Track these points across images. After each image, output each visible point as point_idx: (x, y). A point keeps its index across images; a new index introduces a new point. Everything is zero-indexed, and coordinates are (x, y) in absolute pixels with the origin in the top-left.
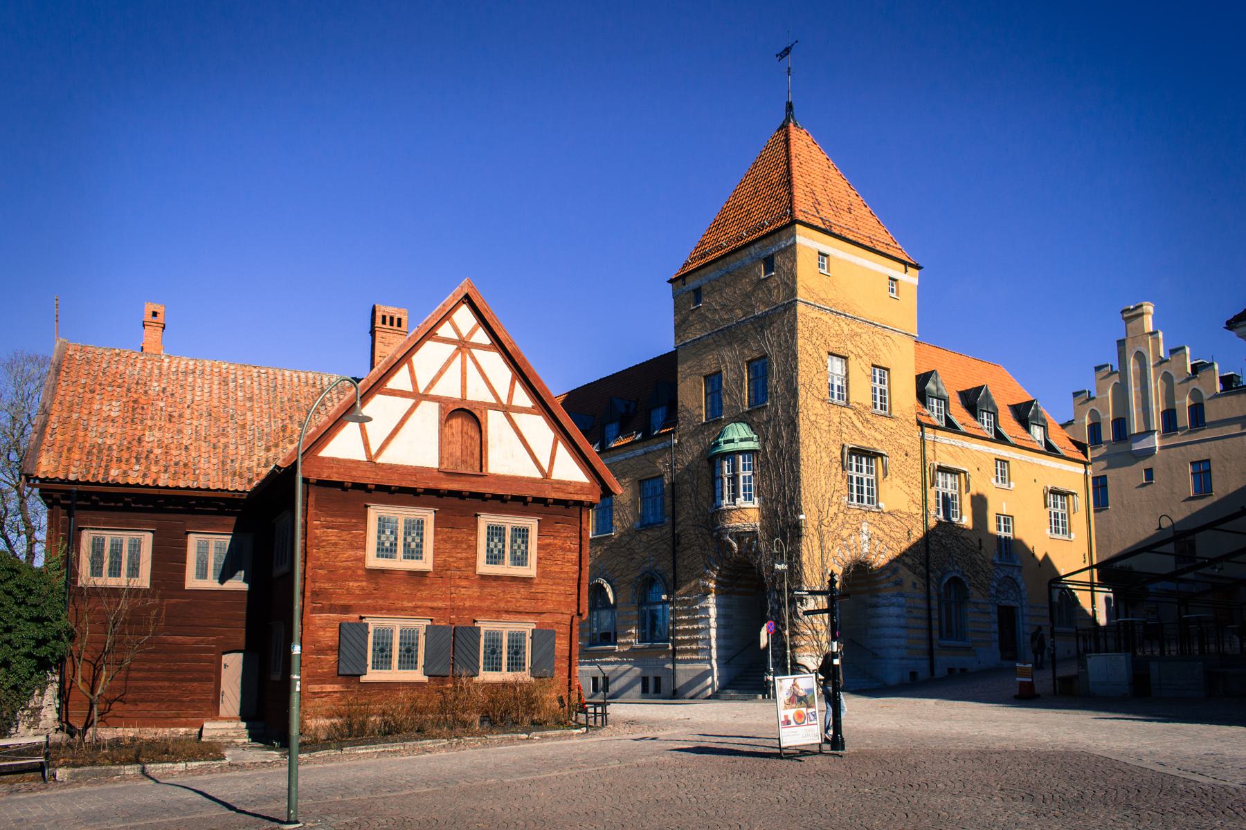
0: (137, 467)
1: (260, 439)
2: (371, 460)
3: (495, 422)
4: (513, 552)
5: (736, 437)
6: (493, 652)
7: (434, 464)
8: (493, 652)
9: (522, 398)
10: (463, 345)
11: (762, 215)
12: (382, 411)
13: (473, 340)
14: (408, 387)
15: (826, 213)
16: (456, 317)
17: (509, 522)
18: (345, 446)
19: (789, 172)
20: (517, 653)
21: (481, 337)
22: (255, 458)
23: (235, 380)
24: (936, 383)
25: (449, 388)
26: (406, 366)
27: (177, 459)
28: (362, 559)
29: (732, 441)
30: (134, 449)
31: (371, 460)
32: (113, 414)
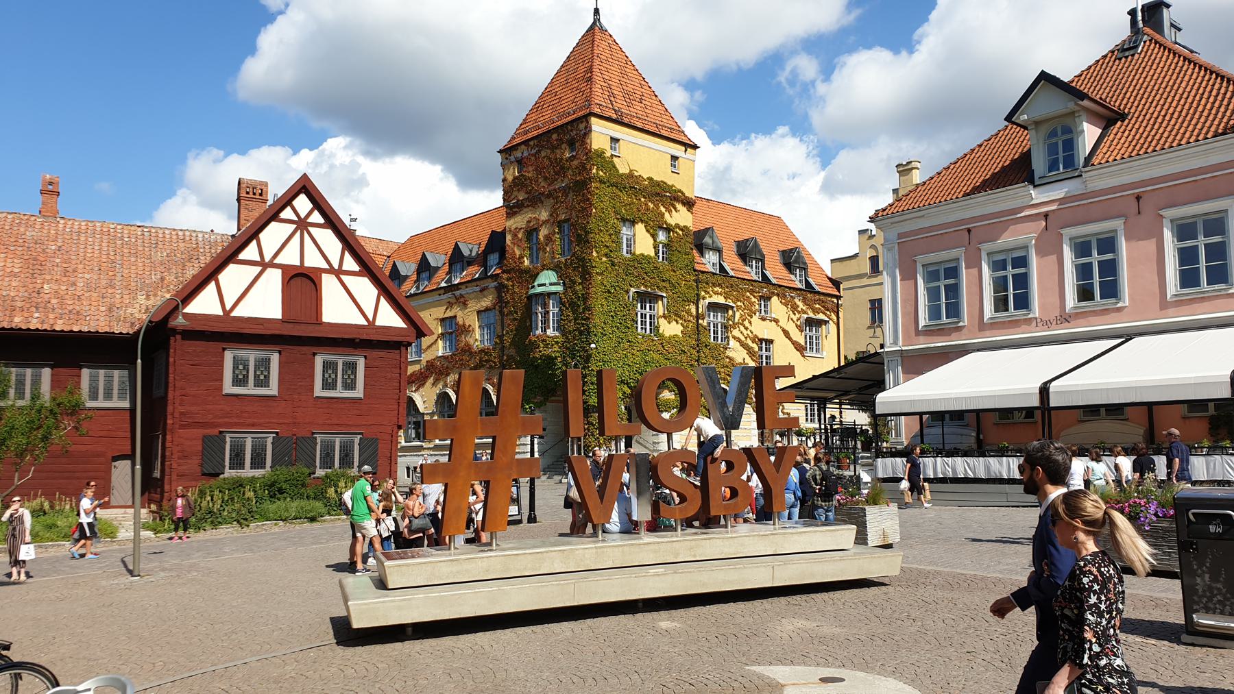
0: (36, 315)
1: (142, 290)
2: (227, 313)
3: (329, 284)
4: (256, 377)
5: (547, 282)
6: (328, 455)
7: (277, 313)
8: (328, 455)
9: (350, 264)
10: (302, 225)
11: (569, 107)
12: (233, 278)
13: (310, 220)
14: (258, 259)
15: (620, 104)
16: (295, 203)
17: (252, 356)
18: (205, 304)
19: (590, 70)
20: (347, 455)
21: (317, 218)
22: (137, 306)
23: (122, 239)
24: (712, 237)
25: (290, 257)
26: (254, 242)
27: (70, 308)
28: (220, 388)
29: (544, 285)
30: (34, 300)
31: (371, 324)
32: (16, 270)
